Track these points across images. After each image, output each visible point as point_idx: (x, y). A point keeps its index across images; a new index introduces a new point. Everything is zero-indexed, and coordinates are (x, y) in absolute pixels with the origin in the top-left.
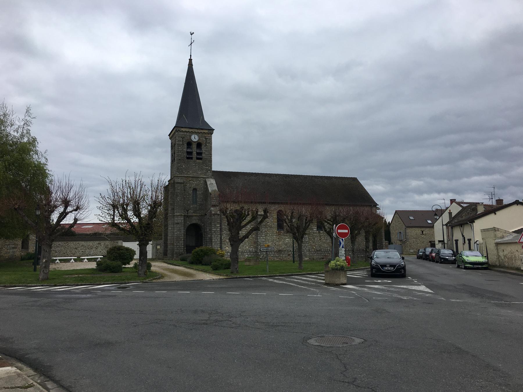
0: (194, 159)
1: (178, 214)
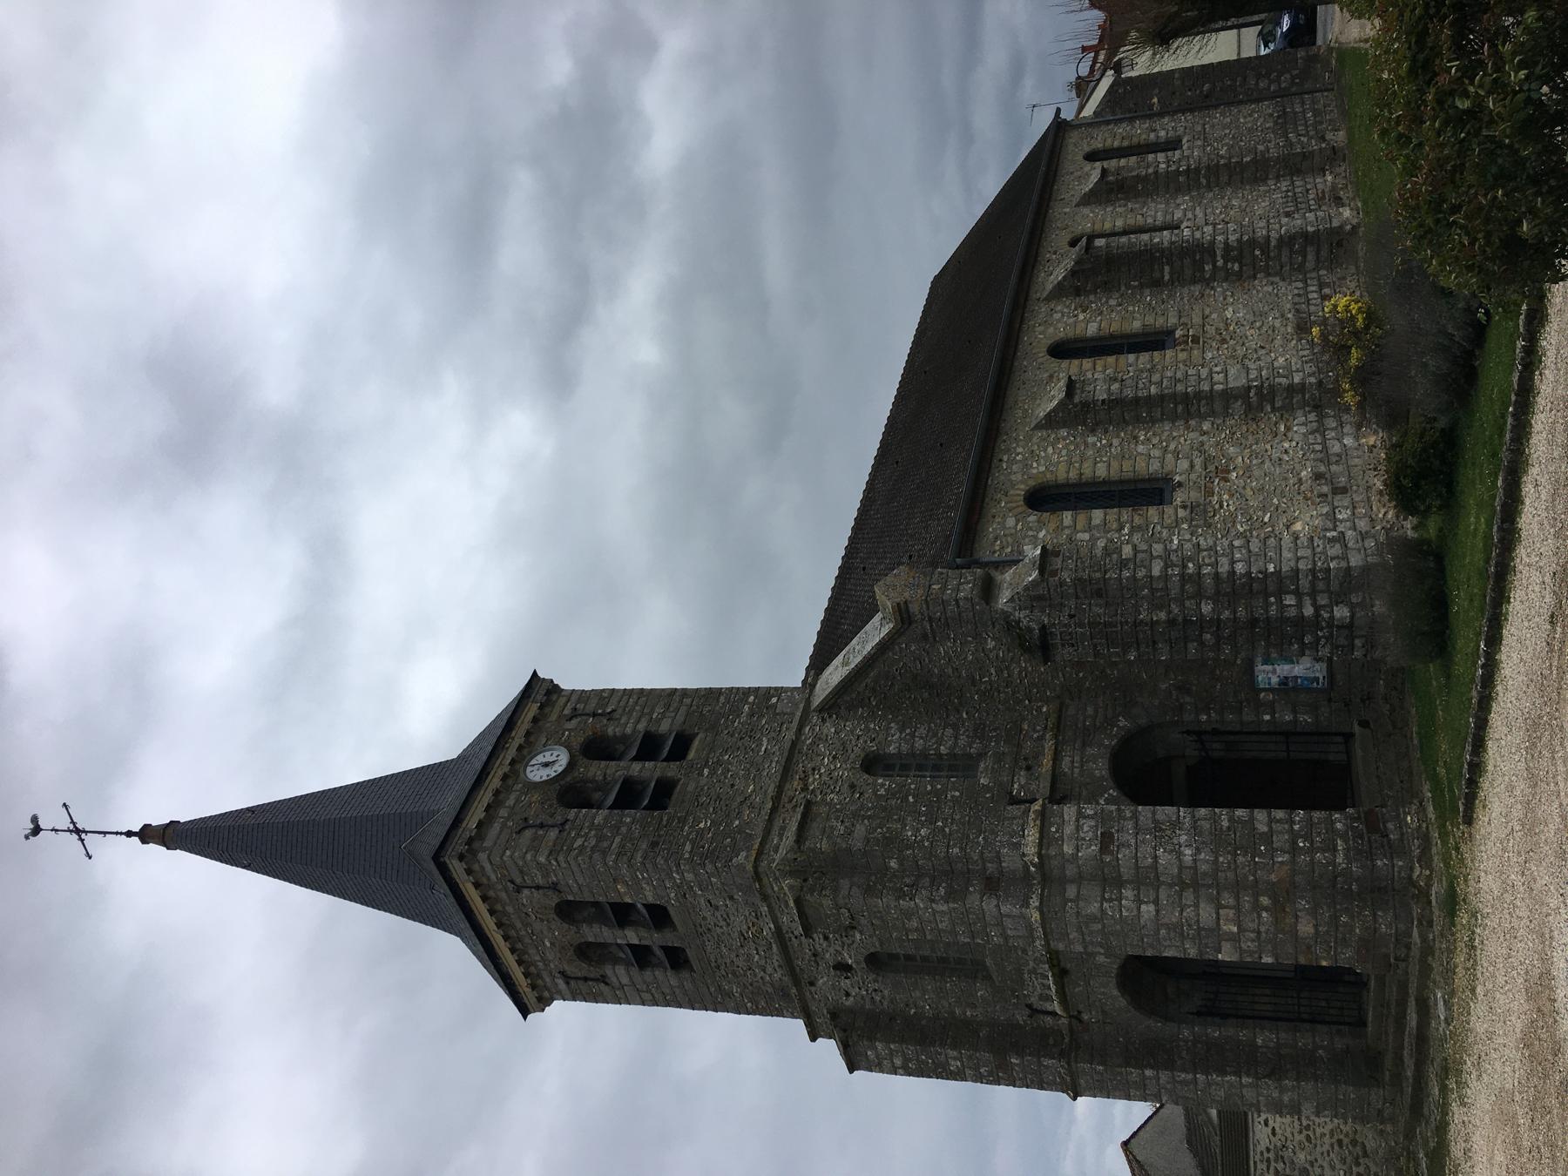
0: (672, 770)
1: (1032, 835)
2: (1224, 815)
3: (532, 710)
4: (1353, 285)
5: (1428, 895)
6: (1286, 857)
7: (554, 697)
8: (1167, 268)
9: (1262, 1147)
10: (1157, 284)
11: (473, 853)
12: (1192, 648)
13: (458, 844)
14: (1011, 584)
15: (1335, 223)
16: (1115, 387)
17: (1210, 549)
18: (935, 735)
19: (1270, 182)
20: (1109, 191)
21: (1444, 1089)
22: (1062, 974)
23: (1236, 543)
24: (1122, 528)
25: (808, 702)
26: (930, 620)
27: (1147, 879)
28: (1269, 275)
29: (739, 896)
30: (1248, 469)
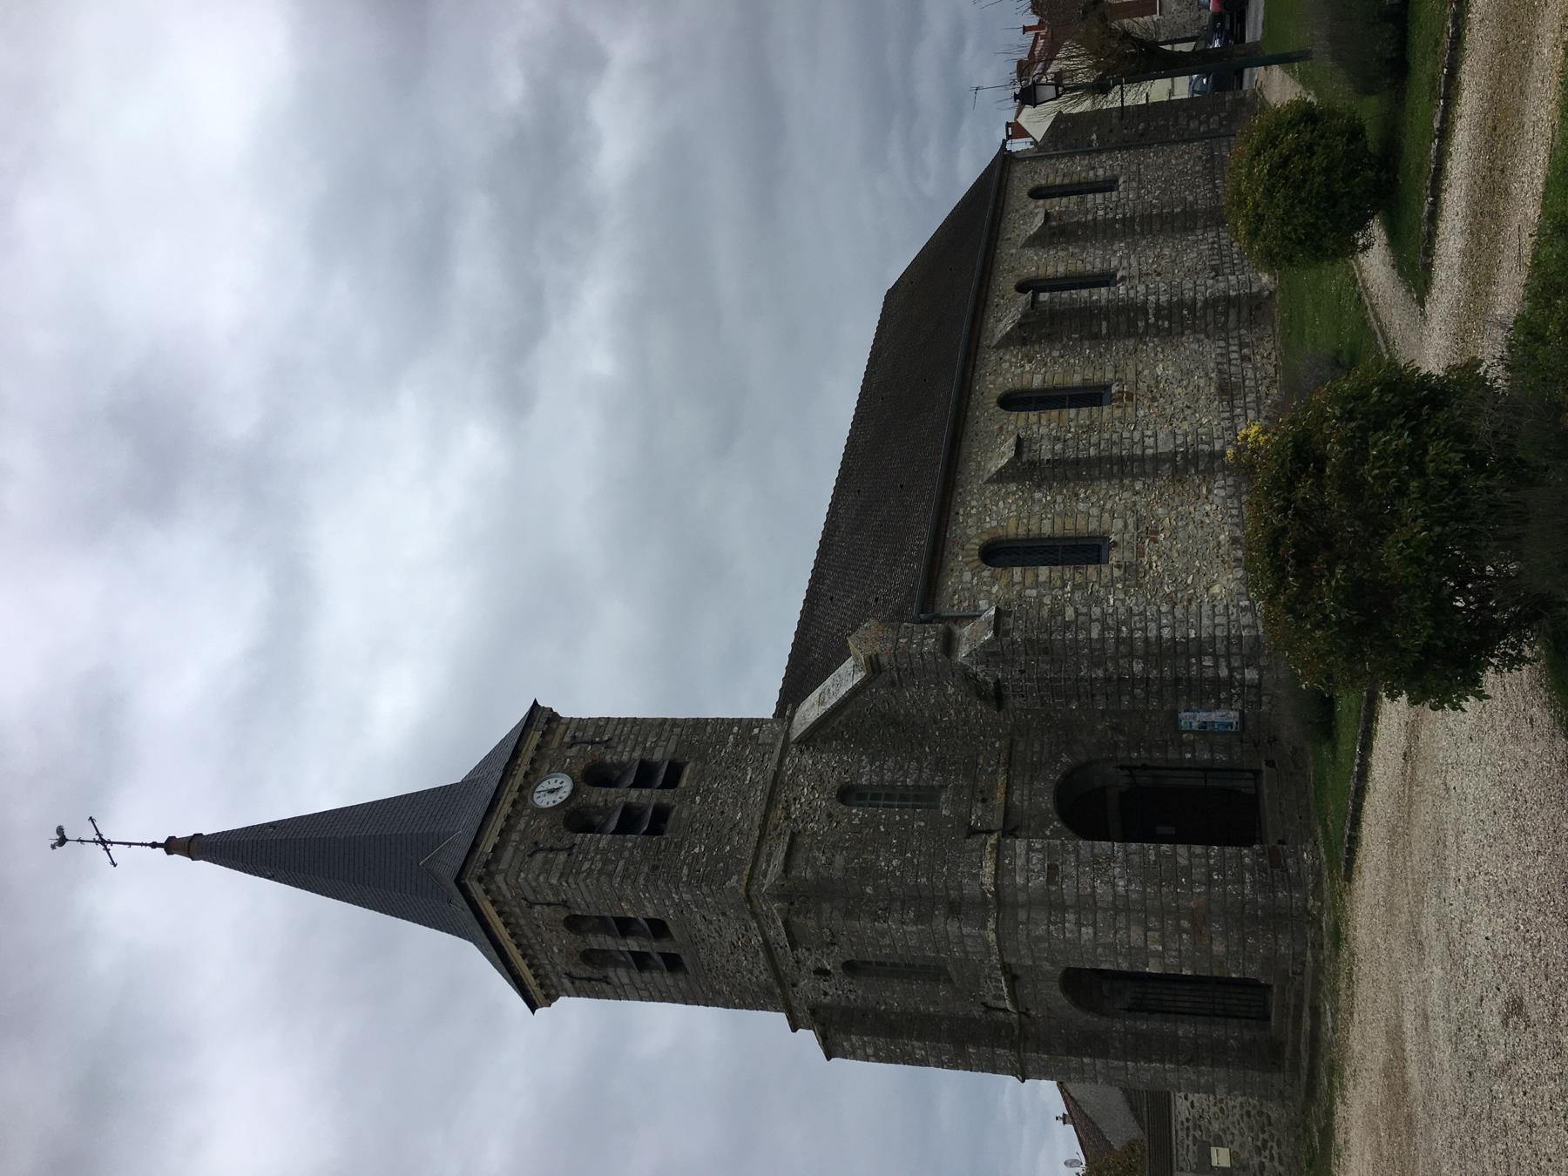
0: (667, 797)
1: (989, 867)
2: (1151, 848)
3: (535, 738)
4: (1269, 346)
5: (1320, 922)
6: (1203, 889)
7: (554, 725)
8: (1104, 324)
9: (1182, 1118)
10: (1096, 337)
11: (490, 875)
12: (1125, 700)
13: (477, 869)
14: (972, 637)
15: (1254, 290)
16: (1058, 447)
17: (1140, 614)
18: (901, 768)
19: (1199, 232)
20: (1054, 234)
21: (1331, 1083)
22: (1013, 979)
23: (1163, 609)
24: (1065, 586)
25: (787, 734)
26: (898, 670)
27: (1086, 906)
28: (1195, 332)
29: (731, 913)
30: (1174, 530)
